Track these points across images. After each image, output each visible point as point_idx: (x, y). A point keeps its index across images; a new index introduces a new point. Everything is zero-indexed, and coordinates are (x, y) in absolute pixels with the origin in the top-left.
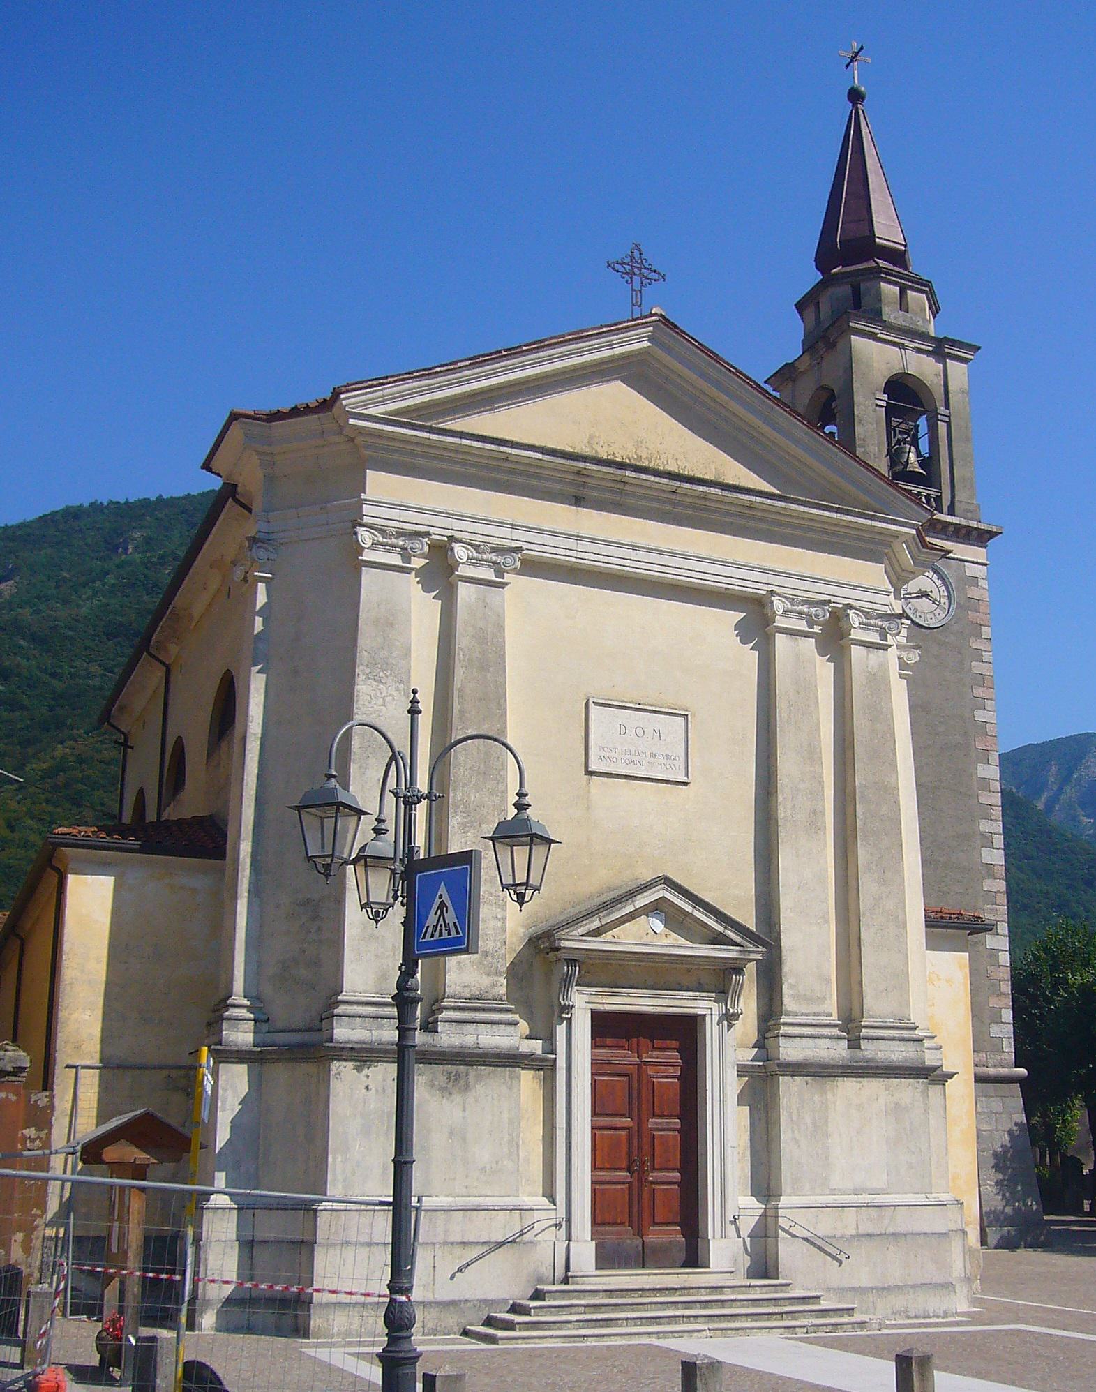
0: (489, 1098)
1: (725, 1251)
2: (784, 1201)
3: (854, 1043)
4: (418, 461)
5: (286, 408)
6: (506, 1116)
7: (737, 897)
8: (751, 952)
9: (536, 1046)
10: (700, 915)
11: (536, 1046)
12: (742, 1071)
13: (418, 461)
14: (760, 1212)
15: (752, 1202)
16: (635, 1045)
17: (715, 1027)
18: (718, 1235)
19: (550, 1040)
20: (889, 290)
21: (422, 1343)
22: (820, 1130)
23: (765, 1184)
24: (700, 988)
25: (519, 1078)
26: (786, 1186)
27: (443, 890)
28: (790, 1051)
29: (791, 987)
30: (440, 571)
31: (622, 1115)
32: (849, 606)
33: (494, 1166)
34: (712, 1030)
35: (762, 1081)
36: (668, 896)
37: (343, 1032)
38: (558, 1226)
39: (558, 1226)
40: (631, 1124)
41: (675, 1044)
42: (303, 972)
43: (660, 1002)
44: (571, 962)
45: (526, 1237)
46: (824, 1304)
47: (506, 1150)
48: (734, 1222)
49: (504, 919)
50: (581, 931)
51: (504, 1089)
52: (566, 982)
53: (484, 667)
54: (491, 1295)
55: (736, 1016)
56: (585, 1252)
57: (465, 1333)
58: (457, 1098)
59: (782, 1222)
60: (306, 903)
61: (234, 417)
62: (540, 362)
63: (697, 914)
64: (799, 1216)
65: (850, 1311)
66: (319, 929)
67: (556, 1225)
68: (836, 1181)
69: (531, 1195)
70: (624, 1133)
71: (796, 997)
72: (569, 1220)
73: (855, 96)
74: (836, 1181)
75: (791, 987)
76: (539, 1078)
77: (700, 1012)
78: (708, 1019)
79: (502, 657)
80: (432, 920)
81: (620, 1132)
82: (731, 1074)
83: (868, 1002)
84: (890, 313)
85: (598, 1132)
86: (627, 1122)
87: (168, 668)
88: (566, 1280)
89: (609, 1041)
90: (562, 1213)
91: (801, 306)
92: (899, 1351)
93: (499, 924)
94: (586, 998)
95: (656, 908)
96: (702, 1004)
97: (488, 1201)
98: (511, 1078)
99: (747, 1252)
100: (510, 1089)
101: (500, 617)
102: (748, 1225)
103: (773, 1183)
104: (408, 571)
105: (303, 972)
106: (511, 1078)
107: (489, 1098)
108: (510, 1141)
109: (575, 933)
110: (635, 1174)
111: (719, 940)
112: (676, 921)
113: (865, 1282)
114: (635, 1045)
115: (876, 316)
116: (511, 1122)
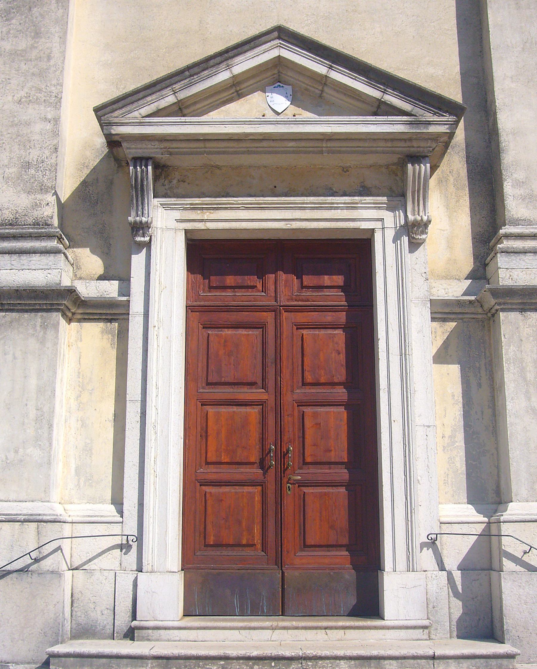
0: (9, 357)
1: (413, 588)
2: (514, 509)
6: (33, 382)
7: (442, 74)
8: (429, 123)
9: (110, 289)
10: (340, 76)
11: (110, 289)
12: (441, 311)
14: (479, 529)
15: (469, 512)
16: (271, 287)
17: (390, 247)
18: (402, 564)
19: (125, 280)
23: (488, 487)
24: (365, 191)
25: (56, 327)
29: (519, 184)
31: (252, 384)
33: (11, 455)
34: (386, 254)
36: (286, 54)
38: (125, 547)
39: (125, 547)
40: (265, 397)
41: (339, 280)
43: (298, 214)
44: (139, 160)
45: (47, 564)
47: (31, 432)
48: (432, 543)
49: (56, 121)
50: (145, 111)
51: (33, 344)
52: (139, 191)
55: (422, 226)
56: (164, 590)
59: (509, 545)
63: (335, 76)
67: (121, 547)
69: (92, 501)
70: (254, 412)
71: (530, 198)
72: (140, 539)
75: (519, 184)
76: (110, 332)
77: (365, 225)
78: (378, 237)
81: (248, 409)
82: (419, 318)
85: (211, 410)
86: (257, 394)
88: (130, 634)
89: (230, 280)
90: (131, 528)
93: (49, 126)
94: (177, 214)
95: (275, 75)
96: (368, 215)
98: (44, 327)
99: (456, 594)
100: (43, 342)
102: (456, 550)
103: (503, 483)
106: (44, 327)
107: (9, 357)
108: (37, 420)
109: (136, 114)
110: (272, 471)
111: (380, 109)
112: (312, 93)
114: (271, 287)
116: (40, 391)
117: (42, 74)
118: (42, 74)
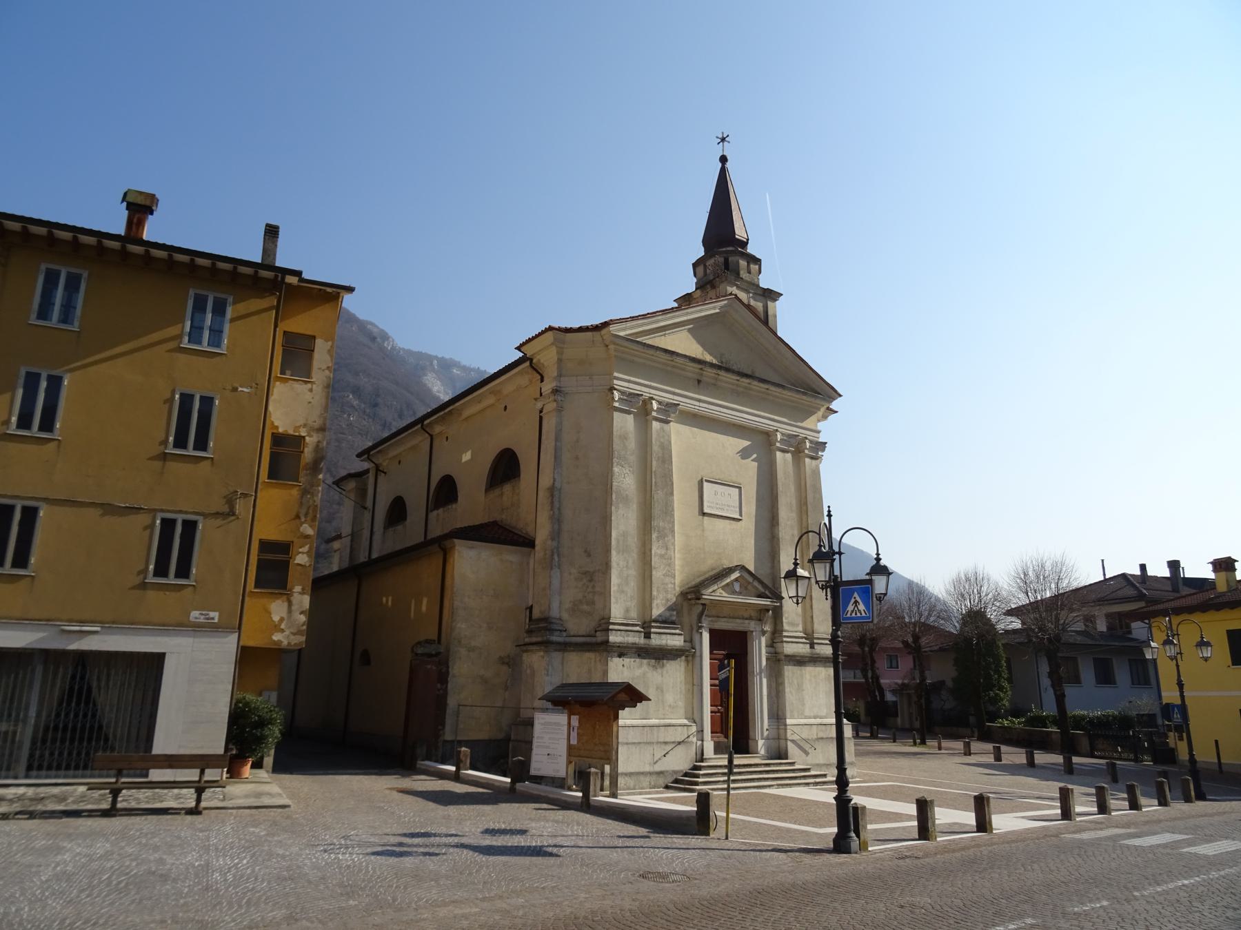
3: (812, 646)
4: (636, 359)
5: (576, 325)
13: (636, 359)
20: (743, 263)
21: (869, 792)
22: (800, 688)
26: (788, 715)
27: (856, 595)
28: (789, 649)
30: (642, 408)
32: (652, 398)
35: (777, 661)
37: (614, 638)
42: (585, 607)
46: (813, 773)
53: (664, 462)
54: (677, 768)
57: (667, 787)
58: (659, 670)
60: (585, 573)
61: (551, 329)
62: (687, 314)
64: (795, 728)
65: (825, 776)
66: (594, 587)
68: (807, 713)
73: (723, 159)
74: (807, 713)
79: (671, 456)
80: (850, 608)
83: (816, 626)
84: (743, 274)
87: (431, 436)
91: (695, 265)
92: (919, 796)
96: (752, 626)
97: (673, 722)
101: (669, 436)
104: (628, 412)
105: (585, 607)
113: (822, 762)
115: (737, 274)
117: (669, 565)
118: (669, 565)
